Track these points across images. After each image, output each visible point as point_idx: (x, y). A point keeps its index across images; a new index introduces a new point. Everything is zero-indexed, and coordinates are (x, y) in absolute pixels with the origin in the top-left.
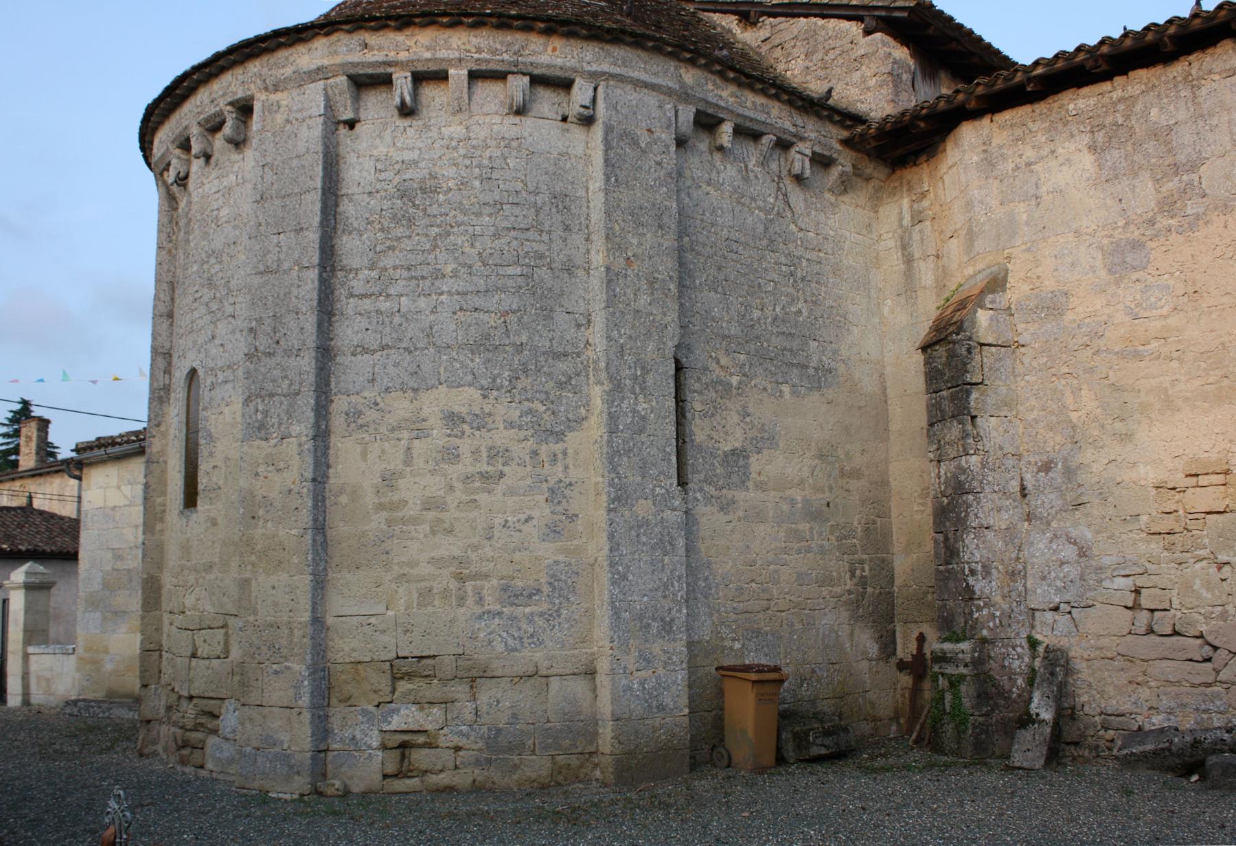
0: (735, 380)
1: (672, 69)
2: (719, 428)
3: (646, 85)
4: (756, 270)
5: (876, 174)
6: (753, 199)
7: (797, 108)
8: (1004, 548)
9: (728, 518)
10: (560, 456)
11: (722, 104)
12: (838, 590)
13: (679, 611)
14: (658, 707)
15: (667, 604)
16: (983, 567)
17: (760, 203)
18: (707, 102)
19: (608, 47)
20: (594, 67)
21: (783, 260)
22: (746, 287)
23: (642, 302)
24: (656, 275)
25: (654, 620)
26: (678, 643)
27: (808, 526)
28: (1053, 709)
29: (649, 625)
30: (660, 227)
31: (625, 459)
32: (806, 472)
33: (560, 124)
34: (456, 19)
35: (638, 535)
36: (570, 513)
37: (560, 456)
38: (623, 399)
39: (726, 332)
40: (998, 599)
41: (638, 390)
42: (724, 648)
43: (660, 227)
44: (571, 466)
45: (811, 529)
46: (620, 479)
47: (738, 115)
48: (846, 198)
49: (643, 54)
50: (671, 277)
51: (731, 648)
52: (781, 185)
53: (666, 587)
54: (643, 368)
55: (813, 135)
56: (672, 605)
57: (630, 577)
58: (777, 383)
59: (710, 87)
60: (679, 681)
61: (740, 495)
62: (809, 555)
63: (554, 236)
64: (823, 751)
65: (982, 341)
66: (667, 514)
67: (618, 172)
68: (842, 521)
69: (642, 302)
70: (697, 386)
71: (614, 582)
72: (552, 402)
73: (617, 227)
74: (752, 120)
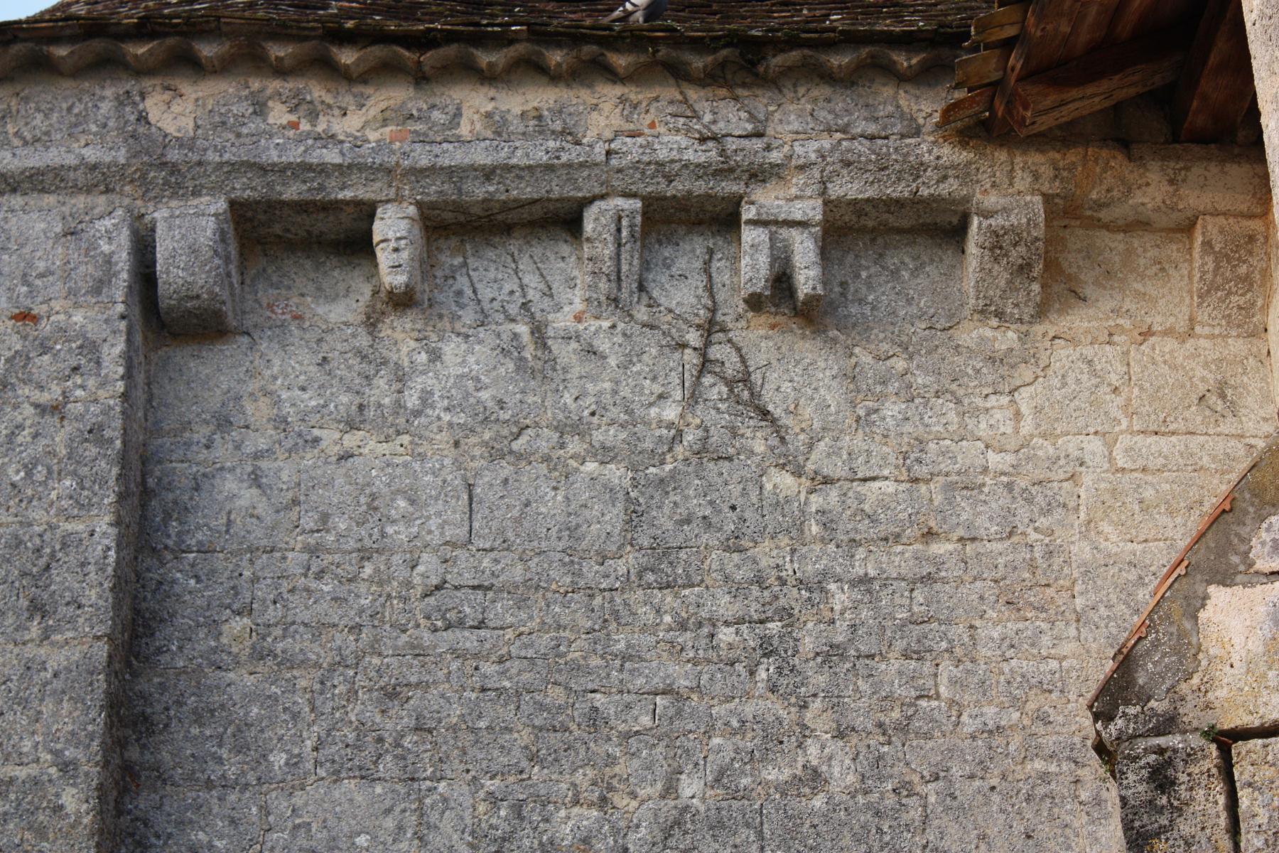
4: (576, 668)
5: (1192, 199)
6: (569, 428)
7: (710, 79)
18: (263, 169)
21: (724, 605)
34: (586, 46)
43: (37, 608)
47: (418, 173)
50: (67, 768)
52: (715, 352)
55: (808, 150)
59: (279, 115)
65: (1229, 722)
74: (488, 173)
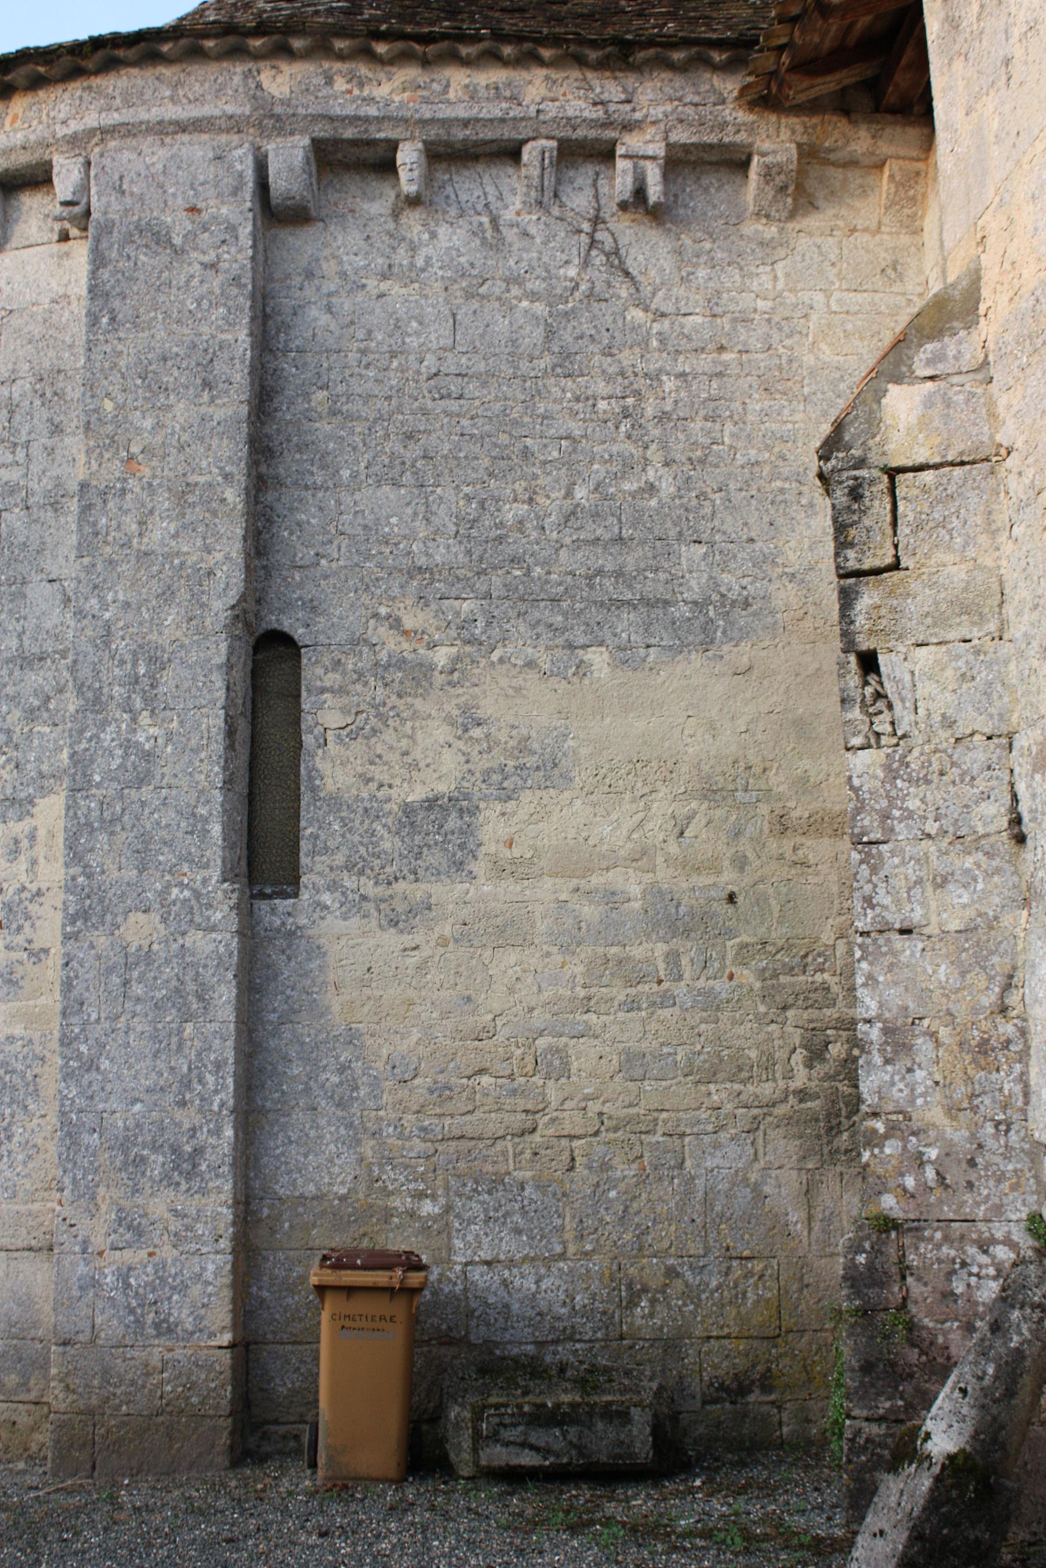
0: (442, 656)
1: (237, 79)
2: (393, 757)
3: (182, 127)
4: (516, 423)
5: (884, 148)
8: (955, 982)
9: (408, 940)
10: (25, 843)
11: (372, 111)
12: (767, 1090)
13: (217, 1132)
14: (157, 1326)
15: (187, 1118)
16: (886, 1031)
17: (537, 285)
18: (331, 119)
19: (96, 81)
20: (74, 126)
22: (486, 462)
23: (157, 535)
24: (193, 478)
25: (155, 1148)
26: (213, 1197)
27: (661, 948)
28: (968, 1428)
29: (143, 1160)
30: (207, 384)
31: (103, 837)
32: (657, 829)
33: (56, 248)
35: (126, 983)
36: (36, 946)
37: (25, 843)
38: (104, 724)
39: (422, 561)
40: (936, 1115)
41: (138, 704)
42: (388, 1214)
43: (207, 384)
44: (42, 861)
45: (673, 958)
46: (89, 876)
47: (423, 123)
48: (812, 222)
49: (166, 71)
50: (227, 477)
51: (412, 1214)
52: (599, 236)
53: (186, 1084)
54: (152, 660)
56: (198, 1120)
57: (105, 1064)
58: (571, 646)
59: (340, 85)
60: (209, 1275)
61: (446, 892)
62: (665, 1013)
63: (36, 449)
64: (528, 1459)
66: (196, 939)
67: (117, 303)
68: (778, 934)
69: (157, 535)
70: (332, 679)
71: (68, 1076)
72: (17, 747)
73: (109, 405)
74: (466, 123)
